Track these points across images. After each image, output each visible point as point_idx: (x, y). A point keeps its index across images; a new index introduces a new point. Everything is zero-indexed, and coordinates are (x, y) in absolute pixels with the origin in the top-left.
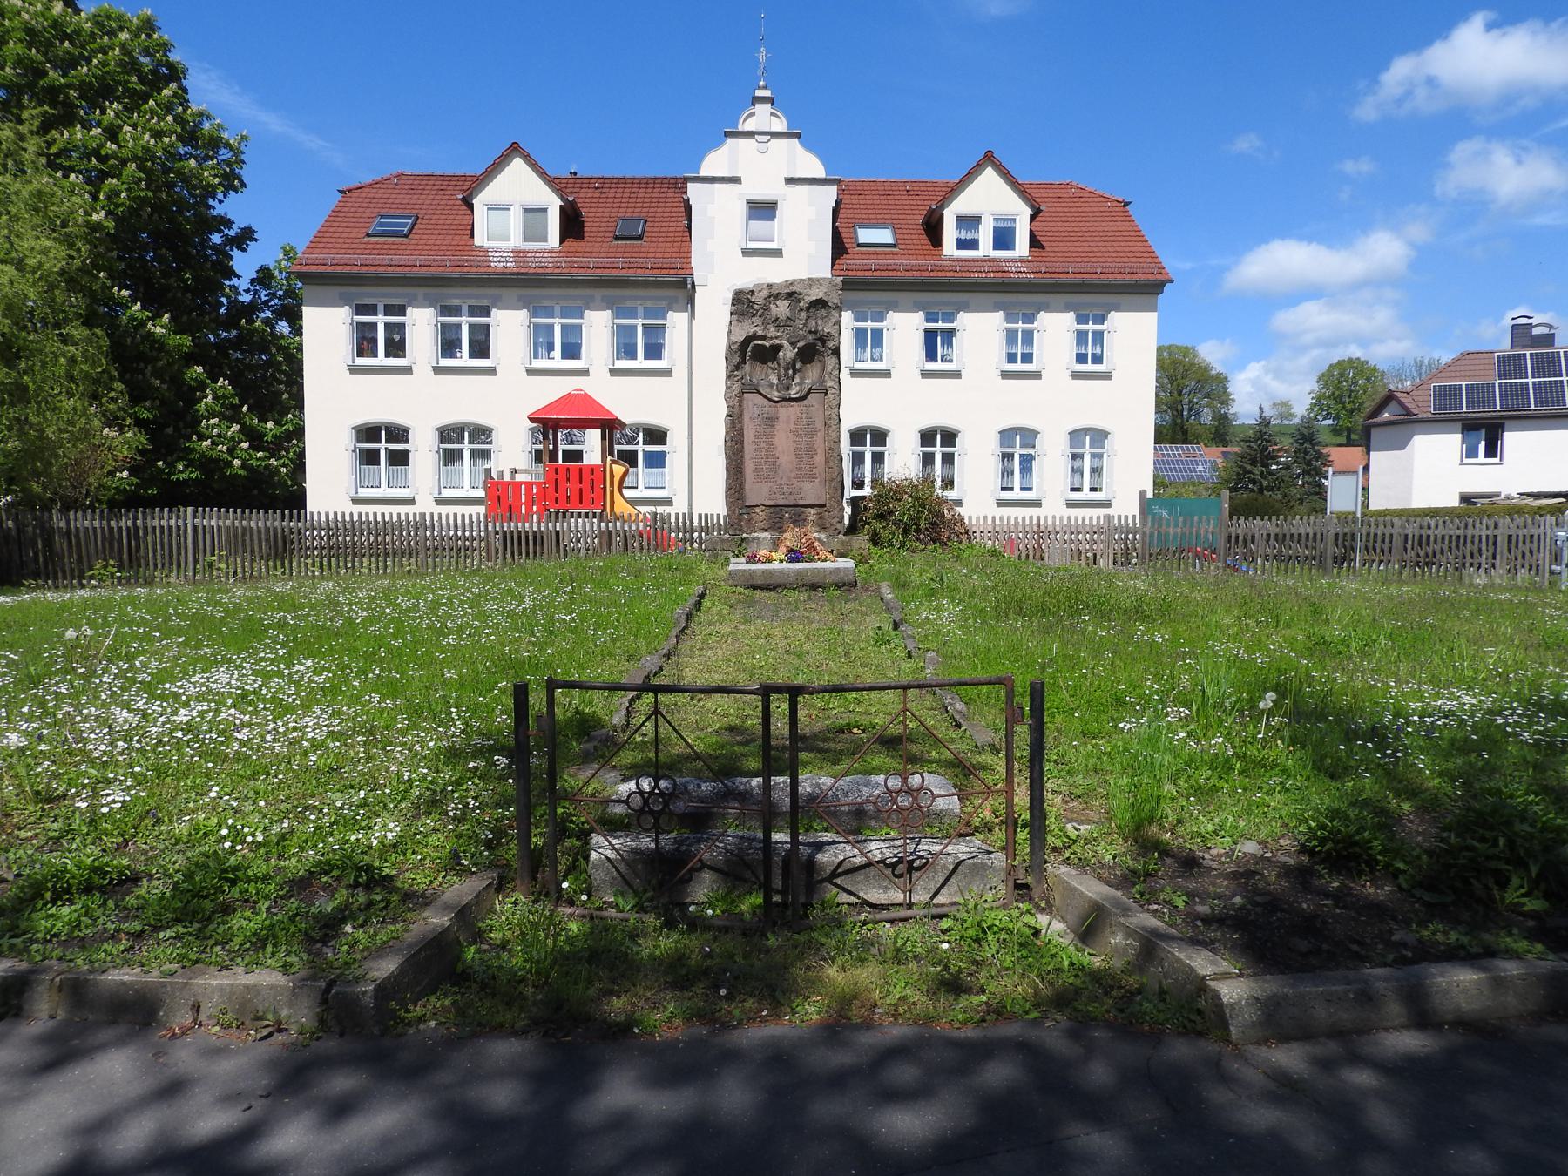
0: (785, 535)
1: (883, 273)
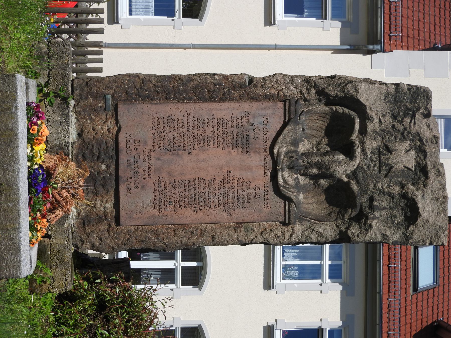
0: (72, 165)
1: (386, 278)
